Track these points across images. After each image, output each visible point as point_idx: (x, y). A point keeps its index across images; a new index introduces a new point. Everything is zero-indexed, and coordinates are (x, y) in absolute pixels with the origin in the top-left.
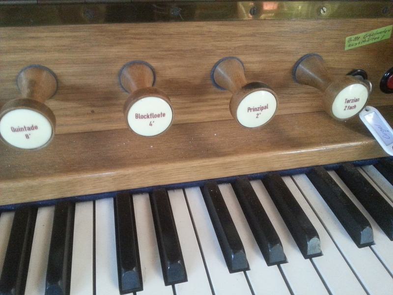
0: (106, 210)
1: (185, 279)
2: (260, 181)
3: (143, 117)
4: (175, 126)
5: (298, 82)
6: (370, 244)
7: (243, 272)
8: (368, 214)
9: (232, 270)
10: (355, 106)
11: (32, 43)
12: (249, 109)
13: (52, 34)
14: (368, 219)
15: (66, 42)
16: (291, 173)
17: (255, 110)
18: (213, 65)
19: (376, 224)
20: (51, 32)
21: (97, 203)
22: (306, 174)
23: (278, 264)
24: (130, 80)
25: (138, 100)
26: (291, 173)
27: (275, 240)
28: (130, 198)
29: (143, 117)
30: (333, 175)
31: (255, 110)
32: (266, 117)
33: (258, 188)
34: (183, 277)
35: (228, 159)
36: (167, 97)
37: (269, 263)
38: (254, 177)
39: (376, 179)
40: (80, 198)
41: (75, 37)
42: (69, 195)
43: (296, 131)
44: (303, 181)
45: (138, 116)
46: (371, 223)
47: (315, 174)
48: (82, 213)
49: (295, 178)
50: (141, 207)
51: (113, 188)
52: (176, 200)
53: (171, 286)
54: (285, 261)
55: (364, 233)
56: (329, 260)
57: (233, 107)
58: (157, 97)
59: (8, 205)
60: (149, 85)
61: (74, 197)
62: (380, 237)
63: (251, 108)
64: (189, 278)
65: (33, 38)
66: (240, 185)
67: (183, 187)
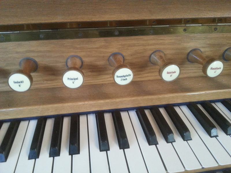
0: (92, 119)
1: (79, 153)
2: (220, 103)
3: (119, 77)
4: (132, 83)
5: (189, 61)
6: (172, 142)
7: (105, 152)
8: (216, 123)
9: (150, 144)
10: (126, 79)
11: (161, 41)
12: (68, 79)
13: (169, 38)
14: (215, 125)
15: (173, 41)
16: (179, 105)
17: (72, 79)
18: (225, 50)
19: (220, 128)
20: (170, 37)
21: (89, 116)
22: (187, 106)
23: (171, 143)
24: (70, 64)
25: (119, 69)
26: (179, 105)
27: (171, 132)
28: (78, 117)
29: (119, 77)
30: (200, 106)
31: (72, 79)
32: (175, 76)
33: (162, 111)
34: (78, 152)
35: (114, 100)
36: (131, 69)
37: (184, 140)
38: (161, 106)
39: (221, 108)
40: (176, 104)
41: (177, 39)
42: (171, 103)
43: (187, 84)
44: (185, 109)
45: (117, 77)
46: (173, 133)
47: (192, 106)
48: (83, 119)
49: (181, 107)
50: (108, 118)
51: (136, 106)
52: (124, 115)
53: (52, 158)
54: (158, 144)
55: (170, 136)
56: (132, 151)
57: (160, 72)
58: (77, 71)
59: (148, 106)
60: (122, 63)
61: (21, 118)
62: (222, 135)
63: (69, 78)
64: (130, 147)
65: (162, 39)
66: (154, 110)
67: (87, 114)
